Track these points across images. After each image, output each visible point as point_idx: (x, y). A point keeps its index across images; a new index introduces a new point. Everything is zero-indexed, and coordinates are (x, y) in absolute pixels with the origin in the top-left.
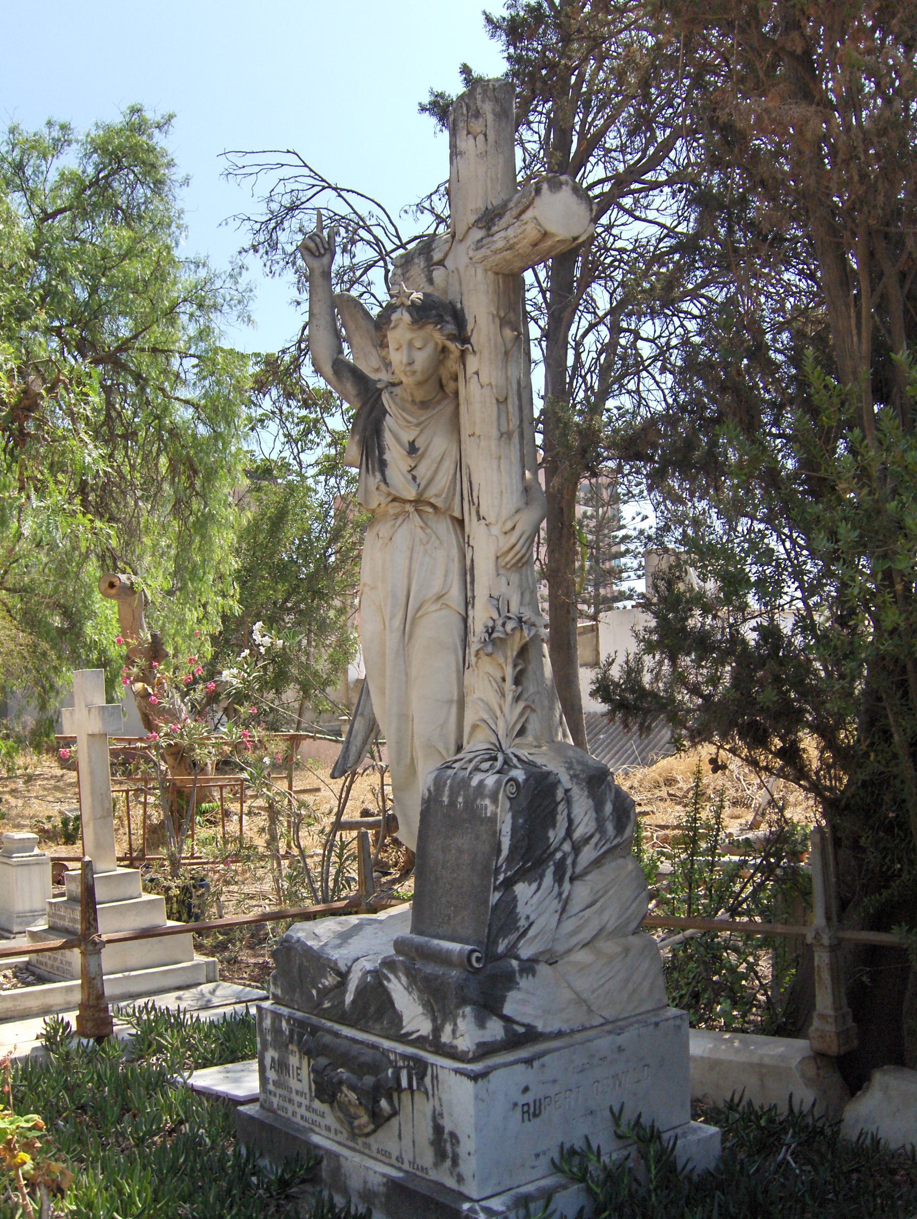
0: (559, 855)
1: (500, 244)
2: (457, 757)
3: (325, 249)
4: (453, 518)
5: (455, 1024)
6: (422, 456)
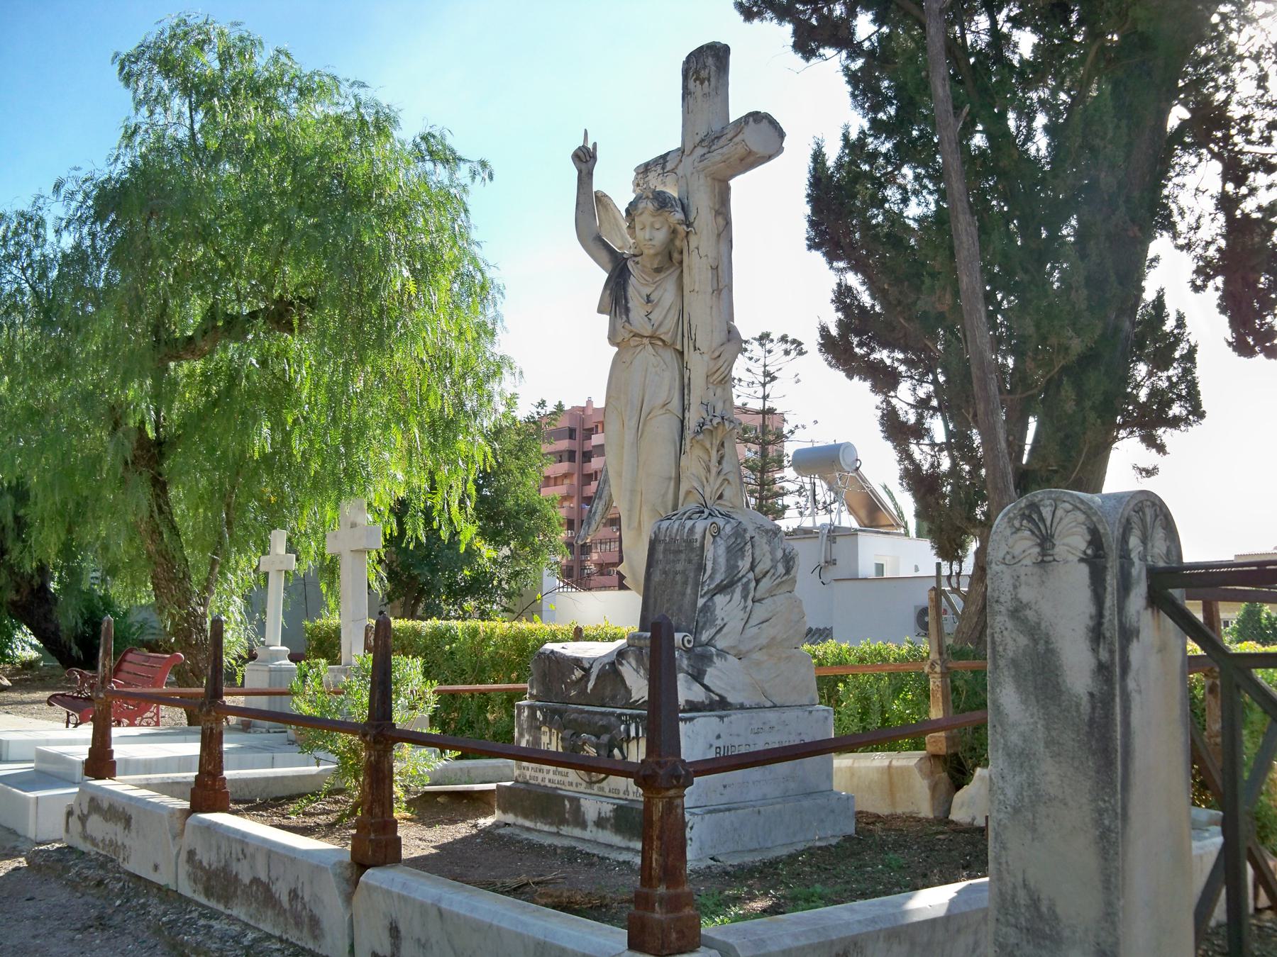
0: (745, 580)
1: (718, 158)
6: (657, 304)
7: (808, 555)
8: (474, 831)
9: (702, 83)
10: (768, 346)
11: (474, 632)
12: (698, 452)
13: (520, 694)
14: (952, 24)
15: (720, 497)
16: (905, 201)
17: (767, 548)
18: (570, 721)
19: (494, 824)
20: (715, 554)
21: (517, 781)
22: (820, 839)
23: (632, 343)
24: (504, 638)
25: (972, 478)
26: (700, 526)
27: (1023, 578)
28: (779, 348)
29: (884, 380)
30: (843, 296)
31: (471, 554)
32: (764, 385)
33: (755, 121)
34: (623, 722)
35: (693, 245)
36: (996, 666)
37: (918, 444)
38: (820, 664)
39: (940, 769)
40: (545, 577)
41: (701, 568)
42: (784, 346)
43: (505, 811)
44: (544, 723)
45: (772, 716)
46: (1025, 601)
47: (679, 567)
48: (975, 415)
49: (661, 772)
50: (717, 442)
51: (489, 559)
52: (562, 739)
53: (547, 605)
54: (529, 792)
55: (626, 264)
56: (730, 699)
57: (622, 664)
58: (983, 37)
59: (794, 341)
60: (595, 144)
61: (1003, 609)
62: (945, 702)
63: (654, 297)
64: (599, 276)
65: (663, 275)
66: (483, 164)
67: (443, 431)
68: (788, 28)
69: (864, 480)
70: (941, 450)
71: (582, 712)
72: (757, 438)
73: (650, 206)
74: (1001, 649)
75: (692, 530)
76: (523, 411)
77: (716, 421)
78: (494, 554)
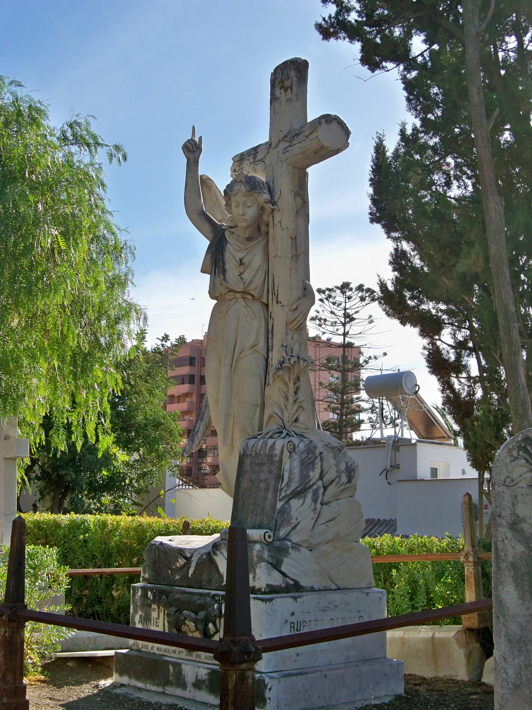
0: (315, 487)
2: (260, 433)
3: (197, 148)
4: (262, 303)
5: (255, 573)
7: (368, 467)
8: (96, 691)
9: (286, 91)
10: (348, 293)
11: (104, 524)
12: (278, 384)
13: (134, 578)
14: (488, 44)
15: (296, 420)
16: (448, 184)
17: (333, 461)
18: (174, 600)
19: (112, 685)
20: (291, 466)
21: (131, 649)
22: (375, 698)
23: (228, 297)
24: (127, 530)
25: (499, 404)
26: (279, 443)
27: (520, 498)
28: (356, 296)
29: (430, 327)
30: (399, 259)
31: (108, 458)
32: (344, 325)
33: (327, 122)
34: (216, 601)
35: (277, 219)
36: (499, 569)
37: (457, 377)
38: (378, 554)
39: (474, 640)
40: (167, 477)
41: (280, 477)
42: (360, 294)
43: (121, 674)
44: (154, 601)
45: (336, 597)
46: (521, 516)
47: (262, 476)
48: (501, 356)
49: (235, 649)
50: (293, 377)
51: (123, 462)
52: (168, 615)
53: (170, 500)
54: (141, 658)
55: (224, 234)
56: (303, 582)
57: (216, 554)
58: (511, 54)
59: (368, 290)
60: (201, 138)
61: (504, 522)
62: (477, 585)
63: (246, 260)
64: (203, 243)
65: (253, 243)
66: (117, 148)
67: (81, 363)
68: (358, 45)
69: (422, 401)
70: (475, 382)
71: (184, 593)
72: (339, 366)
73: (243, 188)
74: (502, 554)
75: (273, 447)
76: (151, 343)
77: (293, 360)
78: (127, 458)
